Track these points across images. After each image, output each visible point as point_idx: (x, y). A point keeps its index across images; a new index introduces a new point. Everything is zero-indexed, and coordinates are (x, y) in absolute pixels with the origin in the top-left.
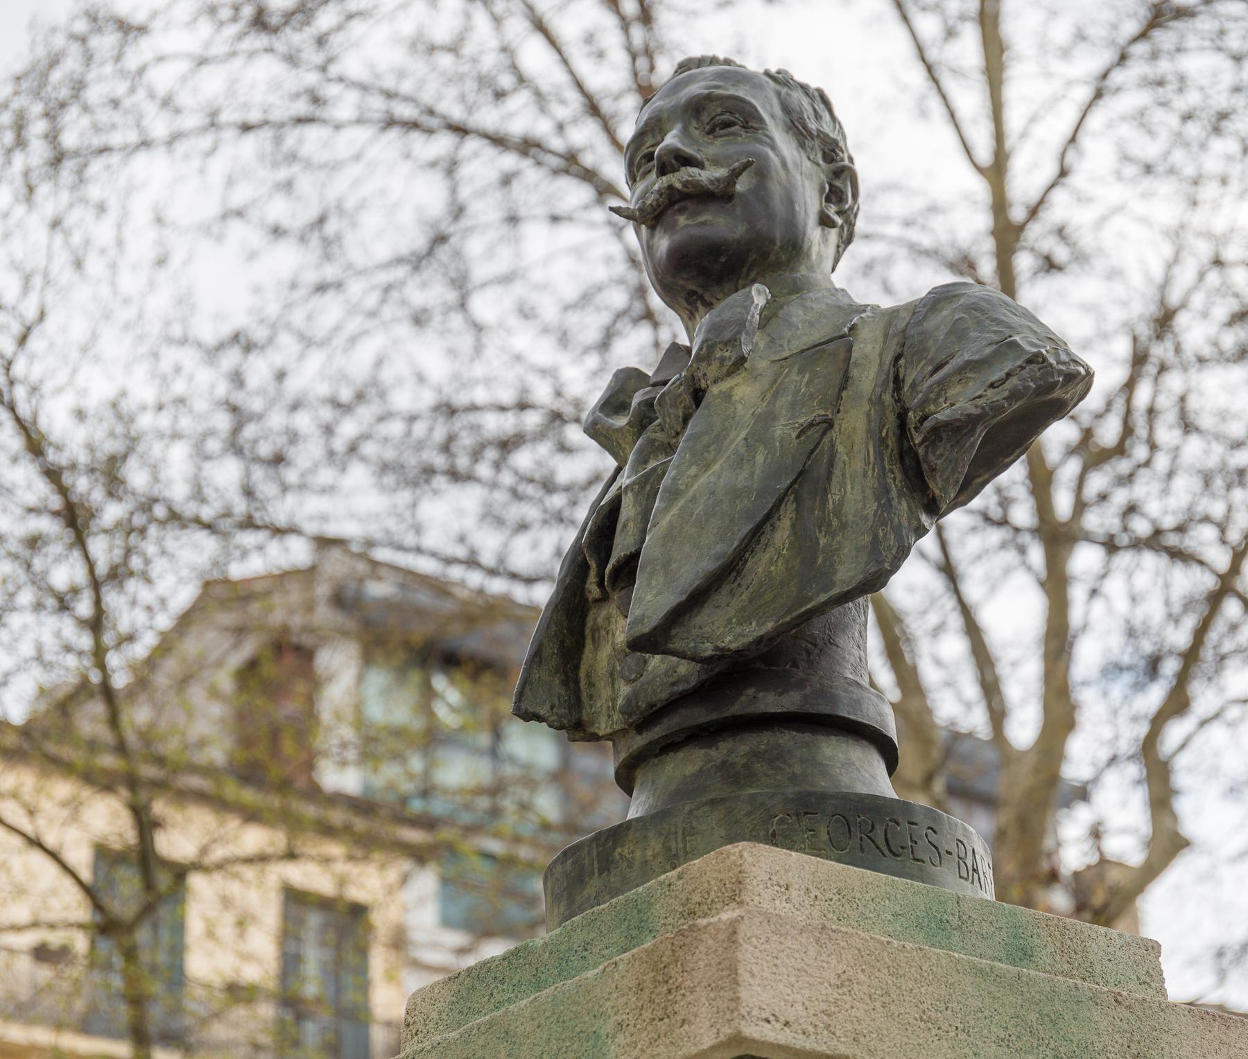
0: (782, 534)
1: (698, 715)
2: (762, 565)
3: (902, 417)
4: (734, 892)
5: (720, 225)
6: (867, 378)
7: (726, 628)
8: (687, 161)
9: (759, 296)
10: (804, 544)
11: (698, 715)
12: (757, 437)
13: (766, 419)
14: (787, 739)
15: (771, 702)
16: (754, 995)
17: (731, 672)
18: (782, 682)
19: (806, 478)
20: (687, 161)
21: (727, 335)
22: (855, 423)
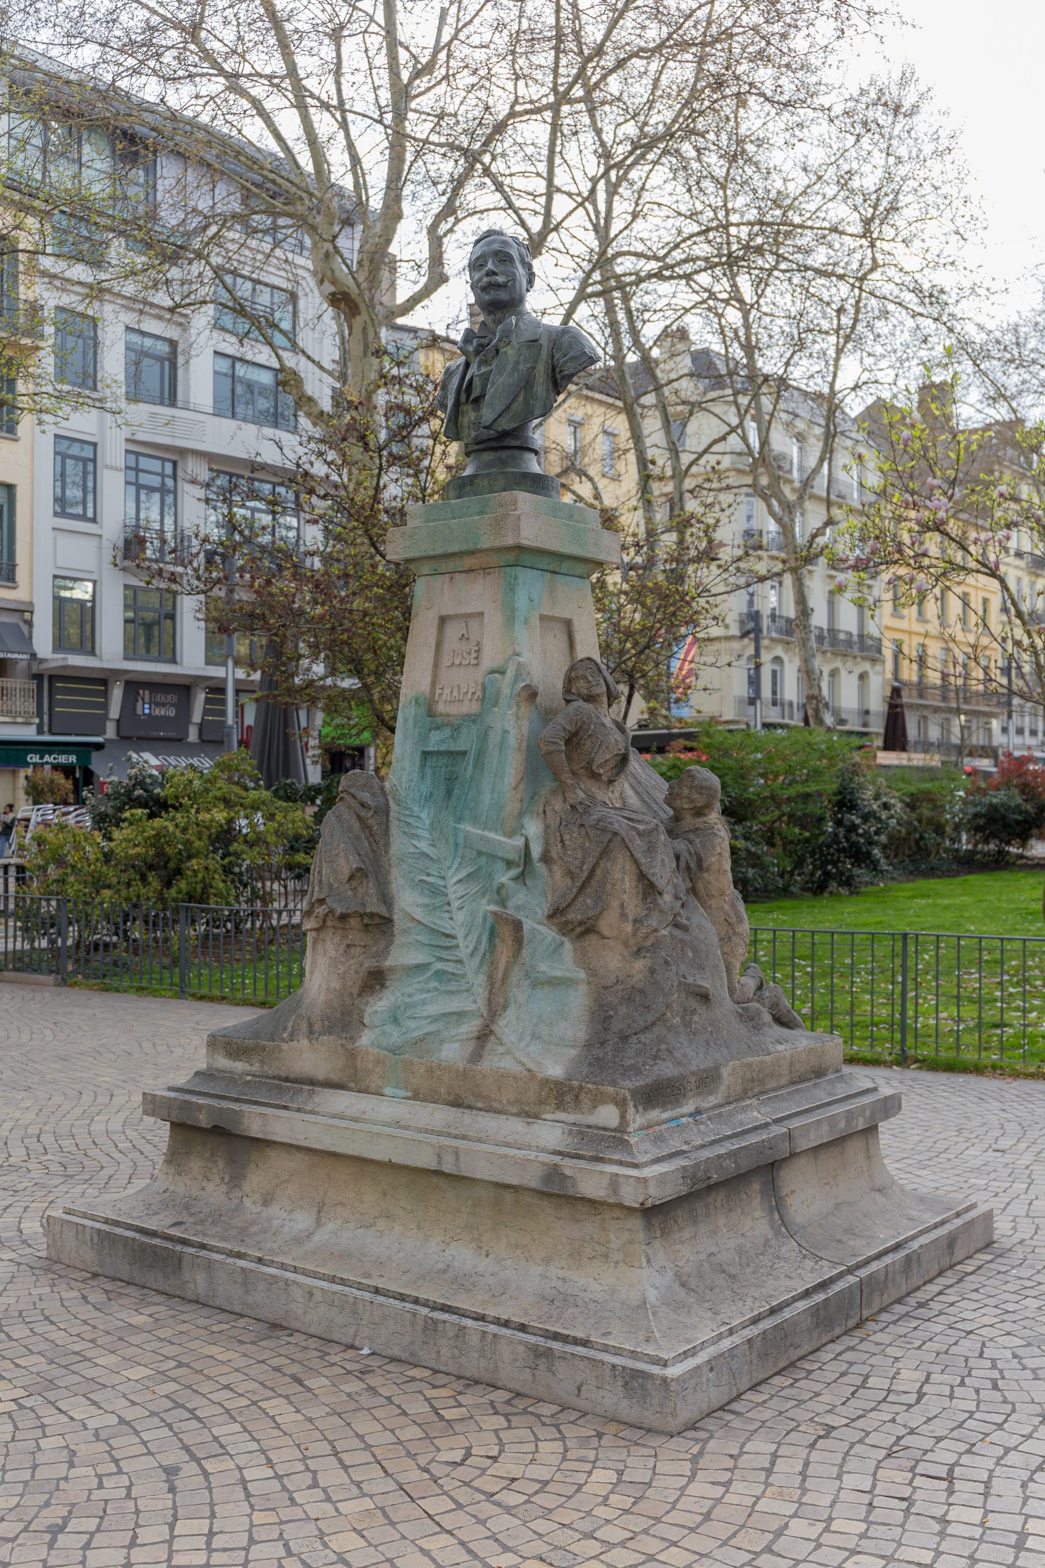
0: (521, 399)
1: (494, 444)
2: (515, 407)
3: (554, 369)
4: (515, 502)
5: (503, 295)
6: (544, 353)
7: (505, 424)
8: (495, 274)
9: (513, 319)
10: (526, 403)
11: (494, 444)
12: (515, 368)
13: (517, 363)
14: (516, 452)
15: (514, 443)
16: (523, 533)
17: (505, 434)
18: (517, 437)
19: (527, 383)
20: (495, 274)
21: (861, 1125)
22: (541, 368)
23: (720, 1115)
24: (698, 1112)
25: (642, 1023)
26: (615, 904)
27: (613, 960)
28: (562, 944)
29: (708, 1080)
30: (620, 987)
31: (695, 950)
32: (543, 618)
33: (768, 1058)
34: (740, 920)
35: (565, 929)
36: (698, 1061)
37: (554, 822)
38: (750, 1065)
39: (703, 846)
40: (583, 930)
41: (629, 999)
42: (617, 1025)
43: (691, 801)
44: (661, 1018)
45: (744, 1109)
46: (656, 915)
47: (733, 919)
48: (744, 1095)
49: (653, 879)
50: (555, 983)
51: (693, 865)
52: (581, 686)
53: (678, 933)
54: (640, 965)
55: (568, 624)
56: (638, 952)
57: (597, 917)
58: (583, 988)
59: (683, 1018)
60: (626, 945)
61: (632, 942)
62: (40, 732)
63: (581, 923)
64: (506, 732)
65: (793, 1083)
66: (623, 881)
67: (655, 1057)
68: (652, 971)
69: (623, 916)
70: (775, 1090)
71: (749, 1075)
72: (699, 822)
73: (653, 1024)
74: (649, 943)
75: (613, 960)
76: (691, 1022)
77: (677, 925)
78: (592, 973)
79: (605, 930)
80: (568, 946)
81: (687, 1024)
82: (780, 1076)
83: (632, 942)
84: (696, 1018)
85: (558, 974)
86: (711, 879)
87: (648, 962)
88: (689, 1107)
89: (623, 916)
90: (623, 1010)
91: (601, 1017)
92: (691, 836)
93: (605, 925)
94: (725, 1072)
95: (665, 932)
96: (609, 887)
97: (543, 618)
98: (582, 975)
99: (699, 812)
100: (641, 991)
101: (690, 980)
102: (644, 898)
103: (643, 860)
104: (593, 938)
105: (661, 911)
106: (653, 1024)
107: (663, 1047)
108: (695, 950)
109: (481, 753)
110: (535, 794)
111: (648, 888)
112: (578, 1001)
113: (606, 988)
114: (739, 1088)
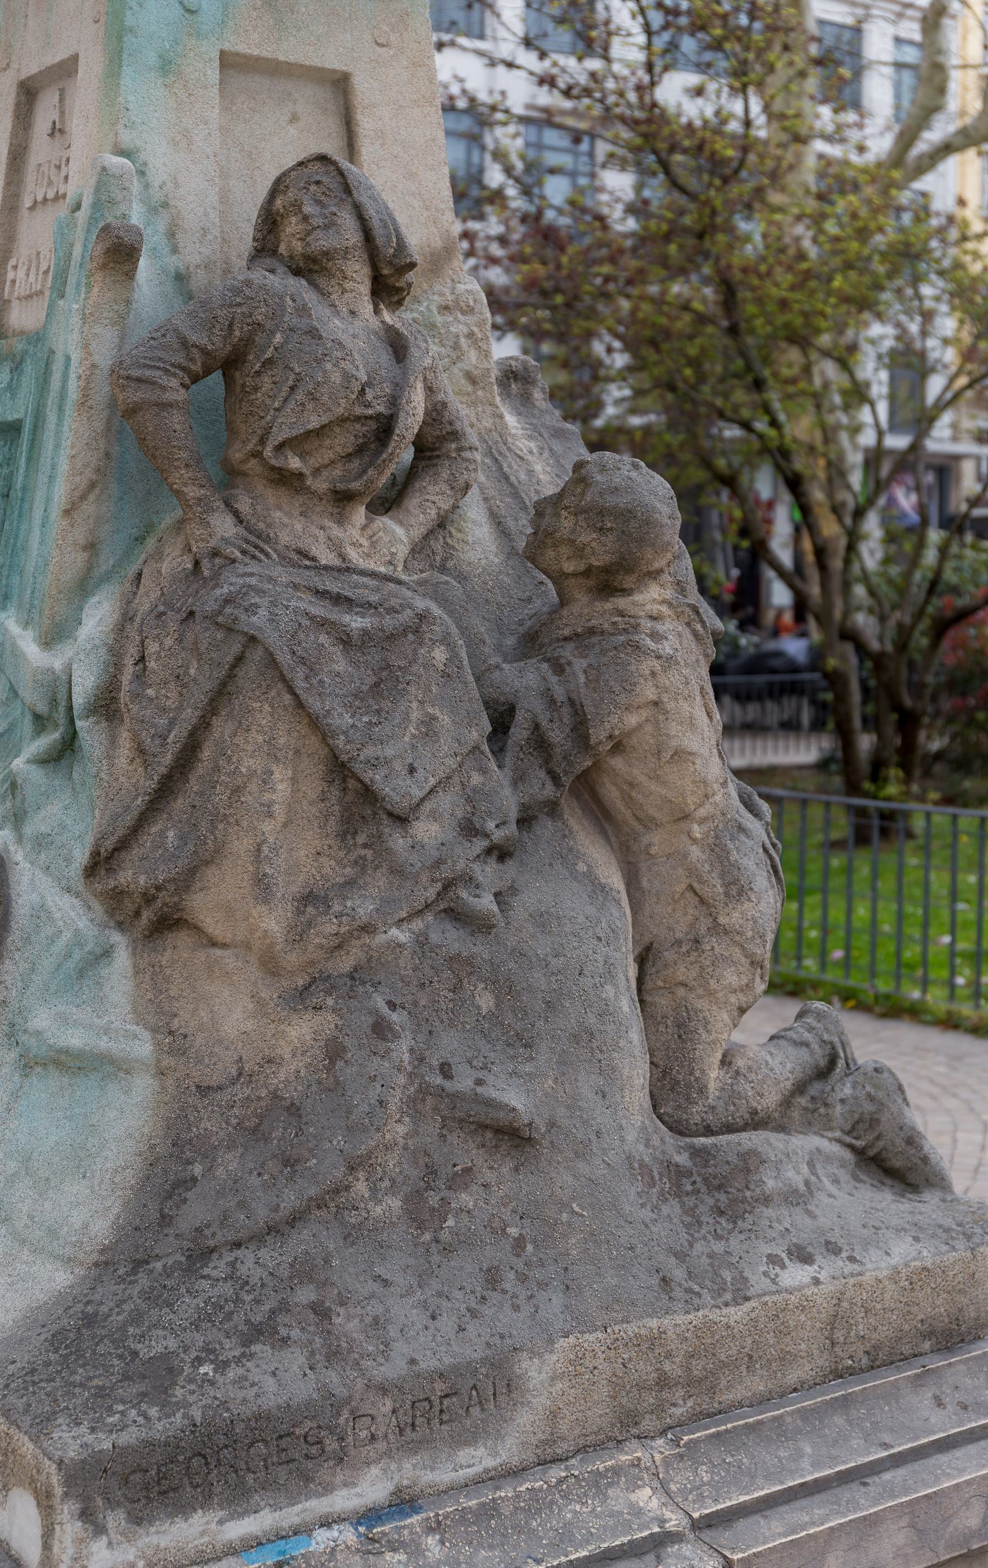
23: (489, 1511)
24: (404, 1502)
25: (262, 1214)
26: (241, 845)
27: (230, 1011)
28: (107, 953)
29: (448, 1404)
30: (240, 1092)
31: (505, 988)
32: (230, 63)
33: (736, 1314)
34: (737, 889)
35: (120, 908)
36: (420, 1337)
37: (144, 604)
38: (654, 1340)
39: (594, 680)
40: (157, 919)
41: (255, 1133)
42: (195, 1212)
43: (579, 552)
44: (333, 1198)
45: (599, 1484)
46: (380, 881)
47: (715, 887)
48: (628, 1425)
49: (377, 778)
50: (69, 1063)
51: (557, 735)
52: (291, 237)
53: (451, 938)
54: (302, 1032)
55: (341, 84)
56: (300, 998)
57: (188, 879)
58: (143, 1086)
59: (415, 1199)
60: (270, 966)
61: (292, 959)
62: (677, 557)
63: (149, 899)
64: (68, 359)
65: (838, 1374)
66: (266, 779)
67: (258, 1333)
68: (334, 1051)
69: (262, 887)
70: (762, 1401)
71: (645, 1370)
72: (601, 612)
73: (295, 1219)
74: (345, 963)
75: (230, 1011)
76: (441, 1213)
77: (456, 915)
78: (173, 1041)
79: (213, 924)
80: (122, 959)
81: (419, 1215)
82: (785, 1359)
83: (292, 959)
84: (466, 1199)
85: (75, 1040)
86: (638, 774)
87: (327, 1022)
88: (372, 1488)
89: (262, 887)
90: (230, 1163)
91: (168, 1177)
92: (567, 652)
93: (204, 906)
94: (536, 1372)
95: (400, 935)
96: (221, 796)
97: (230, 63)
98: (143, 1048)
99: (608, 582)
100: (293, 1110)
101: (463, 1082)
102: (347, 832)
103: (342, 719)
104: (183, 939)
105: (397, 871)
106: (295, 1219)
107: (305, 1295)
108: (505, 988)
109: (38, 426)
110: (149, 528)
111: (359, 805)
112: (125, 1119)
113: (204, 1090)
114: (599, 1414)
